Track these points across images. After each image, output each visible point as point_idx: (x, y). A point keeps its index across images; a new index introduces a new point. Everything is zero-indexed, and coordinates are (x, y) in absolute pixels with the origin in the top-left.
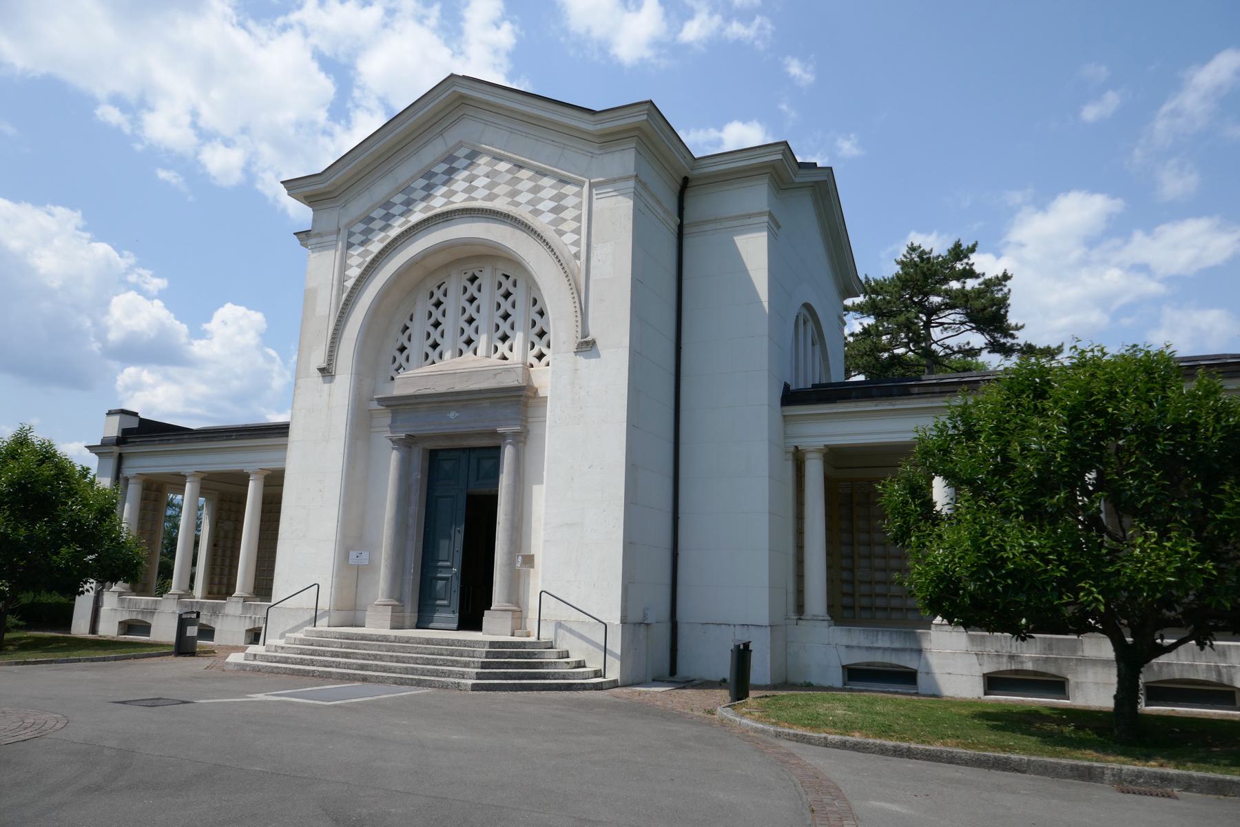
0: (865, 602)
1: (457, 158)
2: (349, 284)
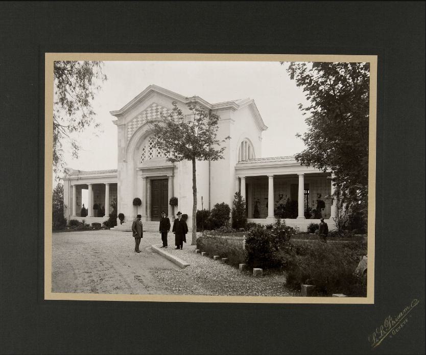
0: (152, 270)
1: (153, 107)
2: (129, 139)
